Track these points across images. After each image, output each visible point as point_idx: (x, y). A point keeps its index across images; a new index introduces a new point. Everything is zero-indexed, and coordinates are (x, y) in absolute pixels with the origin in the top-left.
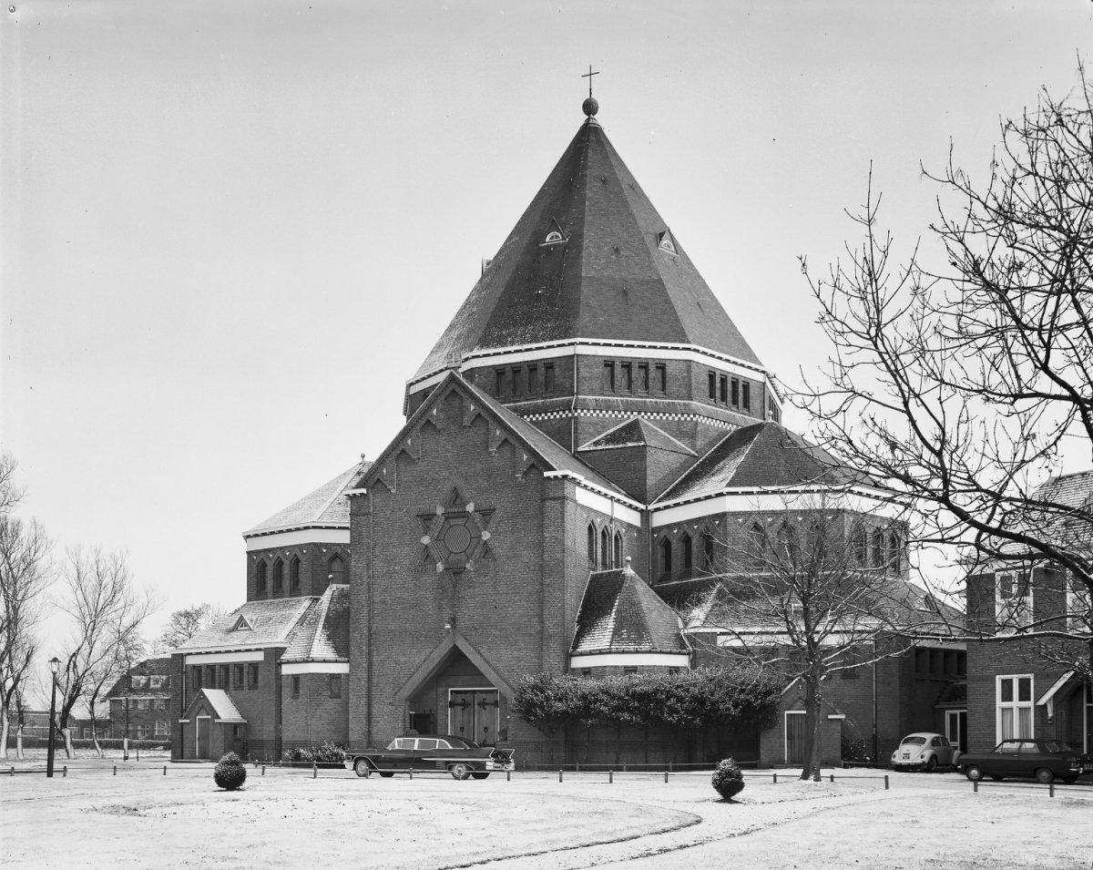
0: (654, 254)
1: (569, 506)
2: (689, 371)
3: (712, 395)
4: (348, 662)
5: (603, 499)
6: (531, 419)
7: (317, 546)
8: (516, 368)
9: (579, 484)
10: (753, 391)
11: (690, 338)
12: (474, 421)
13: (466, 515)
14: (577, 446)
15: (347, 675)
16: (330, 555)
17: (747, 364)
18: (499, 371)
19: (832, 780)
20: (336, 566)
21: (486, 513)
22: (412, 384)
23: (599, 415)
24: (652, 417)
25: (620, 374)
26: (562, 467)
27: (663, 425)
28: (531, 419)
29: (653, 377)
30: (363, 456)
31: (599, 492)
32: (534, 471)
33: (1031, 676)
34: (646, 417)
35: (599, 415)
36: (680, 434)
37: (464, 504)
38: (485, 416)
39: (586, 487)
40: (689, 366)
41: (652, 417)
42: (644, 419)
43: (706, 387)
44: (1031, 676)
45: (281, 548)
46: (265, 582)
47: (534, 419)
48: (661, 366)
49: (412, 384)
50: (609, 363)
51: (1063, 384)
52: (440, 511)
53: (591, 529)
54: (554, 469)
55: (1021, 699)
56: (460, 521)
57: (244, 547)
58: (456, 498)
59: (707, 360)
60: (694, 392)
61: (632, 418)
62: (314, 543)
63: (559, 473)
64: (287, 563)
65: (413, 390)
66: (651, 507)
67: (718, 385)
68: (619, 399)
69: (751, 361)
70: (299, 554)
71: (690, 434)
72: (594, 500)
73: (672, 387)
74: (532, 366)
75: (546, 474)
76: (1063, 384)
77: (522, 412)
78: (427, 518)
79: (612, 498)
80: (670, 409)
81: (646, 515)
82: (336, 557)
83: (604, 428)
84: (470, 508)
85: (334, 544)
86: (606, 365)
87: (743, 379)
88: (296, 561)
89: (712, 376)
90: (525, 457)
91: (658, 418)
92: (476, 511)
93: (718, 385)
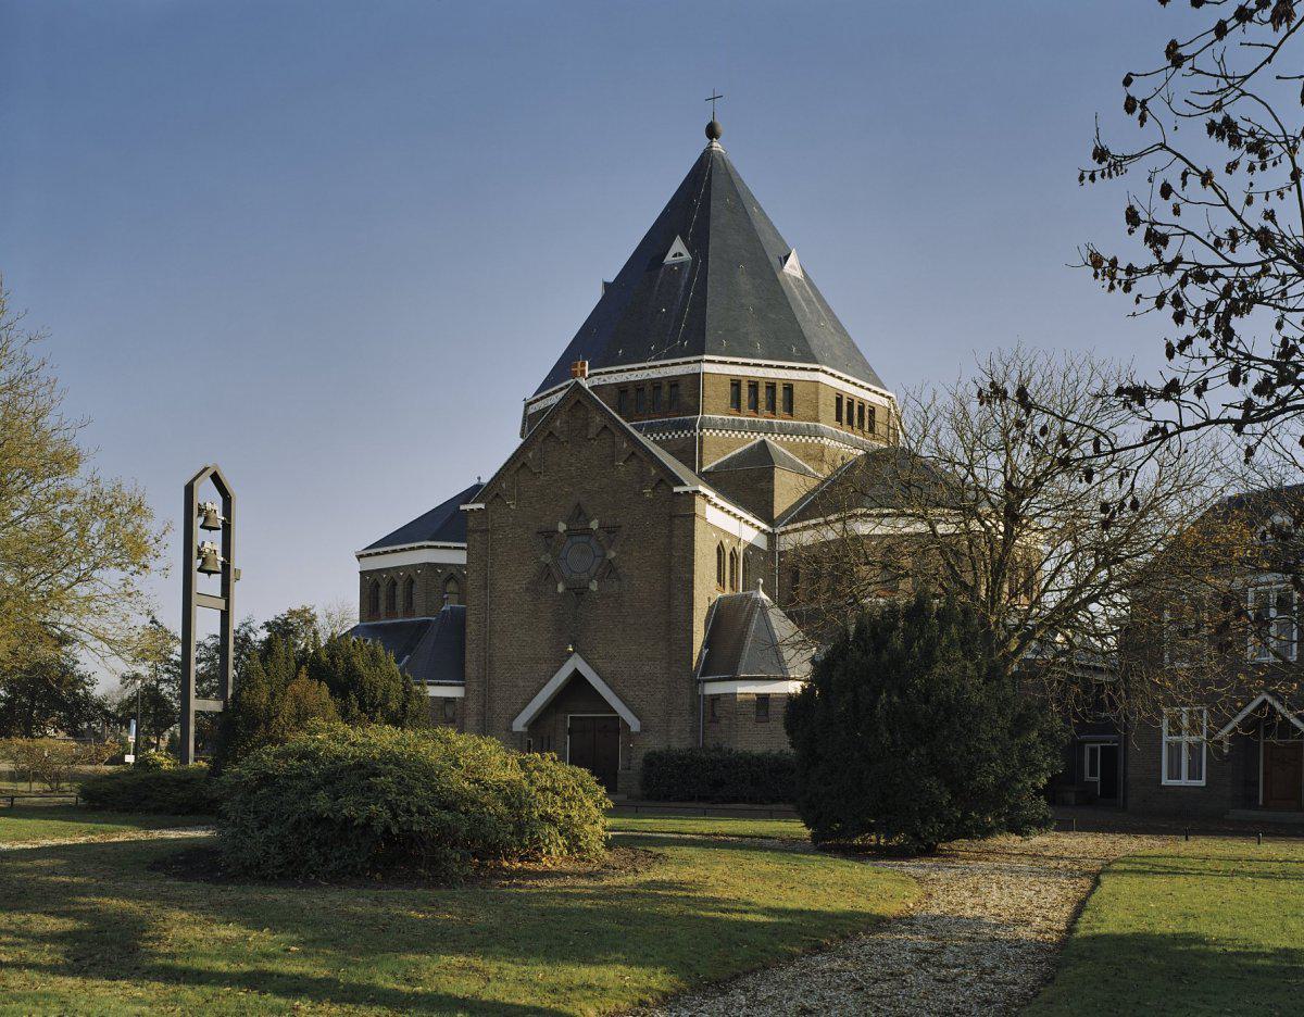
0: (780, 277)
1: (699, 524)
2: (817, 393)
3: (839, 418)
4: (463, 685)
5: (732, 519)
6: (655, 438)
7: (431, 566)
8: (639, 386)
9: (709, 501)
10: (879, 416)
11: (818, 357)
12: (600, 432)
13: (588, 532)
14: (701, 466)
15: (463, 699)
16: (443, 577)
17: (874, 388)
18: (622, 388)
19: (1100, 154)
20: (451, 587)
21: (610, 530)
22: (531, 403)
23: (723, 441)
24: (779, 439)
25: (744, 394)
26: (691, 483)
27: (793, 448)
28: (655, 438)
29: (781, 398)
30: (479, 478)
31: (722, 508)
32: (663, 486)
33: (1165, 781)
34: (773, 438)
35: (723, 441)
36: (808, 457)
37: (588, 522)
38: (610, 428)
39: (716, 505)
40: (817, 388)
41: (779, 439)
42: (770, 439)
43: (833, 410)
44: (1165, 781)
45: (394, 568)
46: (377, 606)
47: (658, 438)
48: (789, 388)
49: (531, 403)
50: (736, 384)
51: (1228, 261)
52: (562, 527)
53: (720, 550)
54: (683, 484)
55: (1179, 745)
56: (585, 539)
57: (355, 568)
58: (579, 514)
59: (833, 381)
60: (821, 415)
61: (759, 439)
62: (428, 563)
63: (689, 488)
64: (400, 583)
65: (532, 410)
66: (777, 531)
67: (845, 408)
68: (746, 419)
69: (878, 386)
70: (413, 574)
71: (818, 456)
72: (723, 523)
73: (798, 408)
74: (656, 384)
75: (676, 490)
76: (1228, 261)
77: (650, 429)
78: (549, 534)
79: (741, 518)
80: (796, 431)
81: (771, 537)
82: (451, 578)
83: (730, 448)
84: (594, 525)
85: (450, 565)
86: (732, 385)
87: (868, 404)
88: (411, 582)
89: (839, 400)
90: (654, 472)
91: (785, 439)
92: (599, 528)
93: (845, 408)
